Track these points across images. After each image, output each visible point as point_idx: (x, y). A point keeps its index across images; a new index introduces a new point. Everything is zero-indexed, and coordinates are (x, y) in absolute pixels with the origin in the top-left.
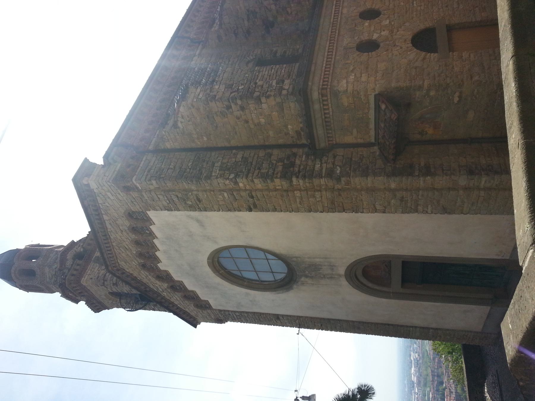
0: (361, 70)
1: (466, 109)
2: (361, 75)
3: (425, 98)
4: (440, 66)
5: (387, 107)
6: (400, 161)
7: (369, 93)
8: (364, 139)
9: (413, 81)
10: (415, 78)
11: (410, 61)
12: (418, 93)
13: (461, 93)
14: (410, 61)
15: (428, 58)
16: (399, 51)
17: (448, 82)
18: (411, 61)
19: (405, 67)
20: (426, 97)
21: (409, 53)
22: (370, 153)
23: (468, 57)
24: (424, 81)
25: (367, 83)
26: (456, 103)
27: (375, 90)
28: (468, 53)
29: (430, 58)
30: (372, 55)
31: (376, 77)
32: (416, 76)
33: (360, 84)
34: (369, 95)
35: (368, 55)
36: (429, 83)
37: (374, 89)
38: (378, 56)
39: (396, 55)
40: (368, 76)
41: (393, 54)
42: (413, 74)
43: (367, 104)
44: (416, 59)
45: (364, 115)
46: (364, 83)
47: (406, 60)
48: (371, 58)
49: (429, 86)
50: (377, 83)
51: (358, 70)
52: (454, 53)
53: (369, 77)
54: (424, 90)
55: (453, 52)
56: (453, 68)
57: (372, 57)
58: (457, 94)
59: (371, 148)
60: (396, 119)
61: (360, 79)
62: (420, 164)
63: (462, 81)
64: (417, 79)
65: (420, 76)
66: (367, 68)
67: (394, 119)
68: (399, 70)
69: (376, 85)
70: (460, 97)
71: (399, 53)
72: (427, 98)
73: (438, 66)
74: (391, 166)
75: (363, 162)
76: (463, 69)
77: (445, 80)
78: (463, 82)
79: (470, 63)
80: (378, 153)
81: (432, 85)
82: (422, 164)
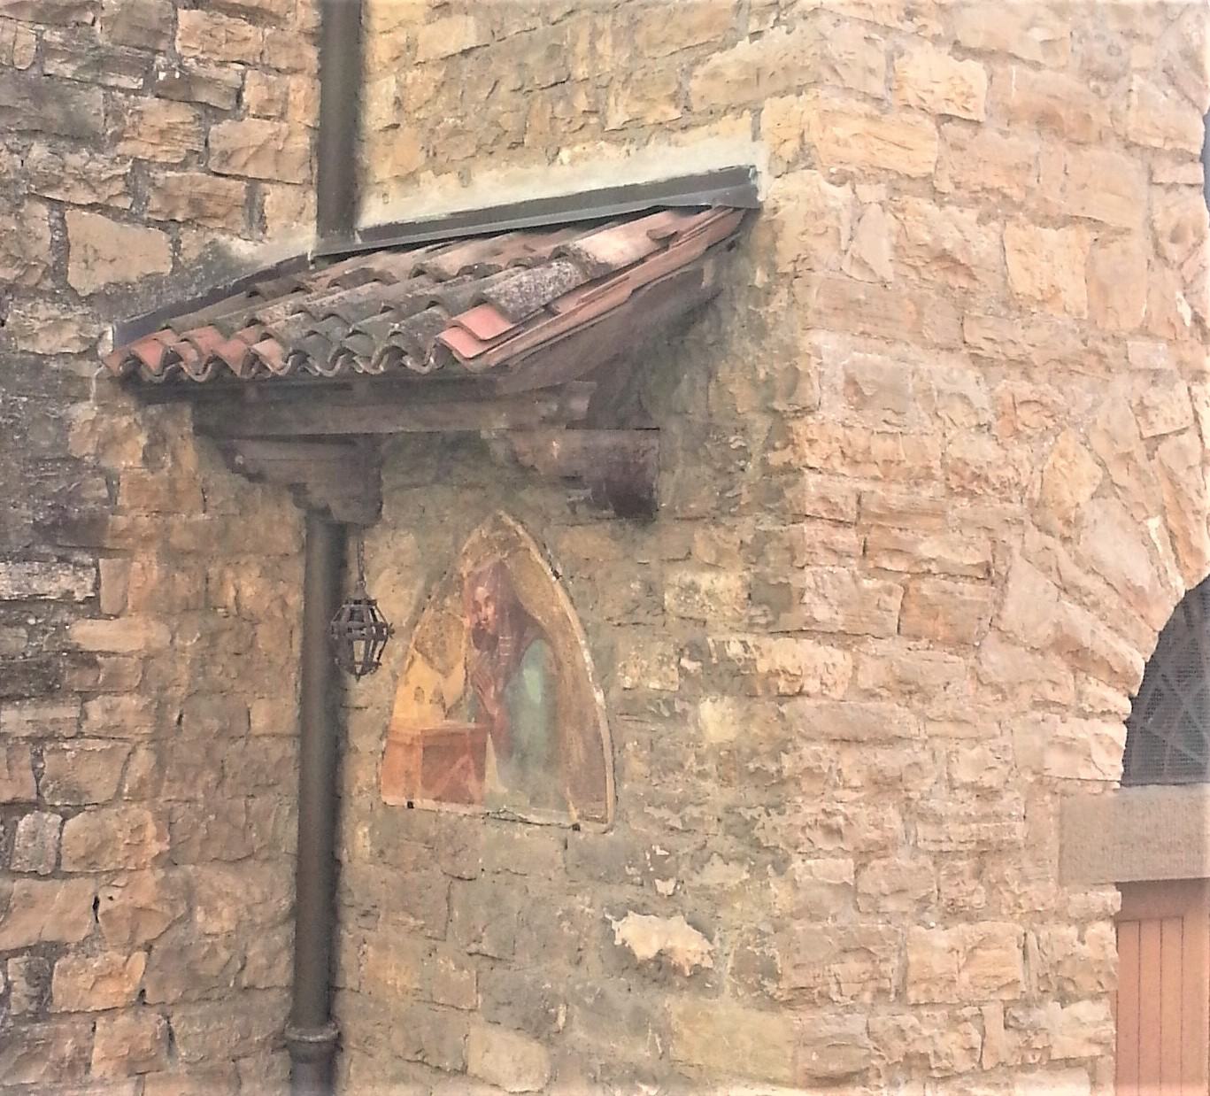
0: (1036, 66)
1: (561, 1020)
2: (976, 54)
3: (681, 653)
4: (986, 794)
5: (601, 275)
6: (143, 440)
7: (773, 109)
8: (396, 126)
9: (848, 539)
10: (885, 564)
11: (1068, 522)
12: (727, 583)
13: (699, 978)
14: (1068, 522)
15: (1080, 694)
16: (1185, 439)
17: (797, 864)
18: (1065, 540)
19: (1009, 473)
20: (692, 658)
21: (1154, 523)
22: (256, 181)
23: (1056, 1055)
24: (845, 638)
25: (879, 100)
26: (611, 934)
27: (791, 166)
28: (1097, 1051)
29: (1087, 717)
30: (1173, 186)
31: (937, 196)
32: (900, 565)
33: (873, 25)
34: (757, 112)
35: (1182, 157)
36: (812, 685)
37: (804, 157)
38: (1156, 245)
39: (1143, 409)
40: (950, 118)
41: (1155, 376)
42: (928, 548)
43: (674, 113)
44: (1087, 582)
45: (582, 103)
46: (878, 61)
47: (1088, 491)
48: (1151, 173)
49: (782, 684)
50: (870, 192)
51: (1038, 34)
52: (1105, 929)
53: (947, 126)
54: (750, 640)
55: (1118, 921)
56: (955, 912)
57: (1151, 183)
58: (687, 946)
59: (312, 197)
60: (445, 351)
61: (936, 39)
62: (92, 608)
63: (802, 997)
64: (870, 576)
65: (895, 603)
66: (1046, 121)
67: (451, 337)
68: (988, 417)
69: (841, 179)
70: (661, 970)
71: (1163, 437)
72: (681, 668)
73: (989, 780)
74: (90, 352)
75: (149, 102)
76: (931, 1004)
77: (833, 832)
78: (789, 1004)
79: (987, 1065)
80: (242, 248)
81: (784, 709)
82: (89, 633)
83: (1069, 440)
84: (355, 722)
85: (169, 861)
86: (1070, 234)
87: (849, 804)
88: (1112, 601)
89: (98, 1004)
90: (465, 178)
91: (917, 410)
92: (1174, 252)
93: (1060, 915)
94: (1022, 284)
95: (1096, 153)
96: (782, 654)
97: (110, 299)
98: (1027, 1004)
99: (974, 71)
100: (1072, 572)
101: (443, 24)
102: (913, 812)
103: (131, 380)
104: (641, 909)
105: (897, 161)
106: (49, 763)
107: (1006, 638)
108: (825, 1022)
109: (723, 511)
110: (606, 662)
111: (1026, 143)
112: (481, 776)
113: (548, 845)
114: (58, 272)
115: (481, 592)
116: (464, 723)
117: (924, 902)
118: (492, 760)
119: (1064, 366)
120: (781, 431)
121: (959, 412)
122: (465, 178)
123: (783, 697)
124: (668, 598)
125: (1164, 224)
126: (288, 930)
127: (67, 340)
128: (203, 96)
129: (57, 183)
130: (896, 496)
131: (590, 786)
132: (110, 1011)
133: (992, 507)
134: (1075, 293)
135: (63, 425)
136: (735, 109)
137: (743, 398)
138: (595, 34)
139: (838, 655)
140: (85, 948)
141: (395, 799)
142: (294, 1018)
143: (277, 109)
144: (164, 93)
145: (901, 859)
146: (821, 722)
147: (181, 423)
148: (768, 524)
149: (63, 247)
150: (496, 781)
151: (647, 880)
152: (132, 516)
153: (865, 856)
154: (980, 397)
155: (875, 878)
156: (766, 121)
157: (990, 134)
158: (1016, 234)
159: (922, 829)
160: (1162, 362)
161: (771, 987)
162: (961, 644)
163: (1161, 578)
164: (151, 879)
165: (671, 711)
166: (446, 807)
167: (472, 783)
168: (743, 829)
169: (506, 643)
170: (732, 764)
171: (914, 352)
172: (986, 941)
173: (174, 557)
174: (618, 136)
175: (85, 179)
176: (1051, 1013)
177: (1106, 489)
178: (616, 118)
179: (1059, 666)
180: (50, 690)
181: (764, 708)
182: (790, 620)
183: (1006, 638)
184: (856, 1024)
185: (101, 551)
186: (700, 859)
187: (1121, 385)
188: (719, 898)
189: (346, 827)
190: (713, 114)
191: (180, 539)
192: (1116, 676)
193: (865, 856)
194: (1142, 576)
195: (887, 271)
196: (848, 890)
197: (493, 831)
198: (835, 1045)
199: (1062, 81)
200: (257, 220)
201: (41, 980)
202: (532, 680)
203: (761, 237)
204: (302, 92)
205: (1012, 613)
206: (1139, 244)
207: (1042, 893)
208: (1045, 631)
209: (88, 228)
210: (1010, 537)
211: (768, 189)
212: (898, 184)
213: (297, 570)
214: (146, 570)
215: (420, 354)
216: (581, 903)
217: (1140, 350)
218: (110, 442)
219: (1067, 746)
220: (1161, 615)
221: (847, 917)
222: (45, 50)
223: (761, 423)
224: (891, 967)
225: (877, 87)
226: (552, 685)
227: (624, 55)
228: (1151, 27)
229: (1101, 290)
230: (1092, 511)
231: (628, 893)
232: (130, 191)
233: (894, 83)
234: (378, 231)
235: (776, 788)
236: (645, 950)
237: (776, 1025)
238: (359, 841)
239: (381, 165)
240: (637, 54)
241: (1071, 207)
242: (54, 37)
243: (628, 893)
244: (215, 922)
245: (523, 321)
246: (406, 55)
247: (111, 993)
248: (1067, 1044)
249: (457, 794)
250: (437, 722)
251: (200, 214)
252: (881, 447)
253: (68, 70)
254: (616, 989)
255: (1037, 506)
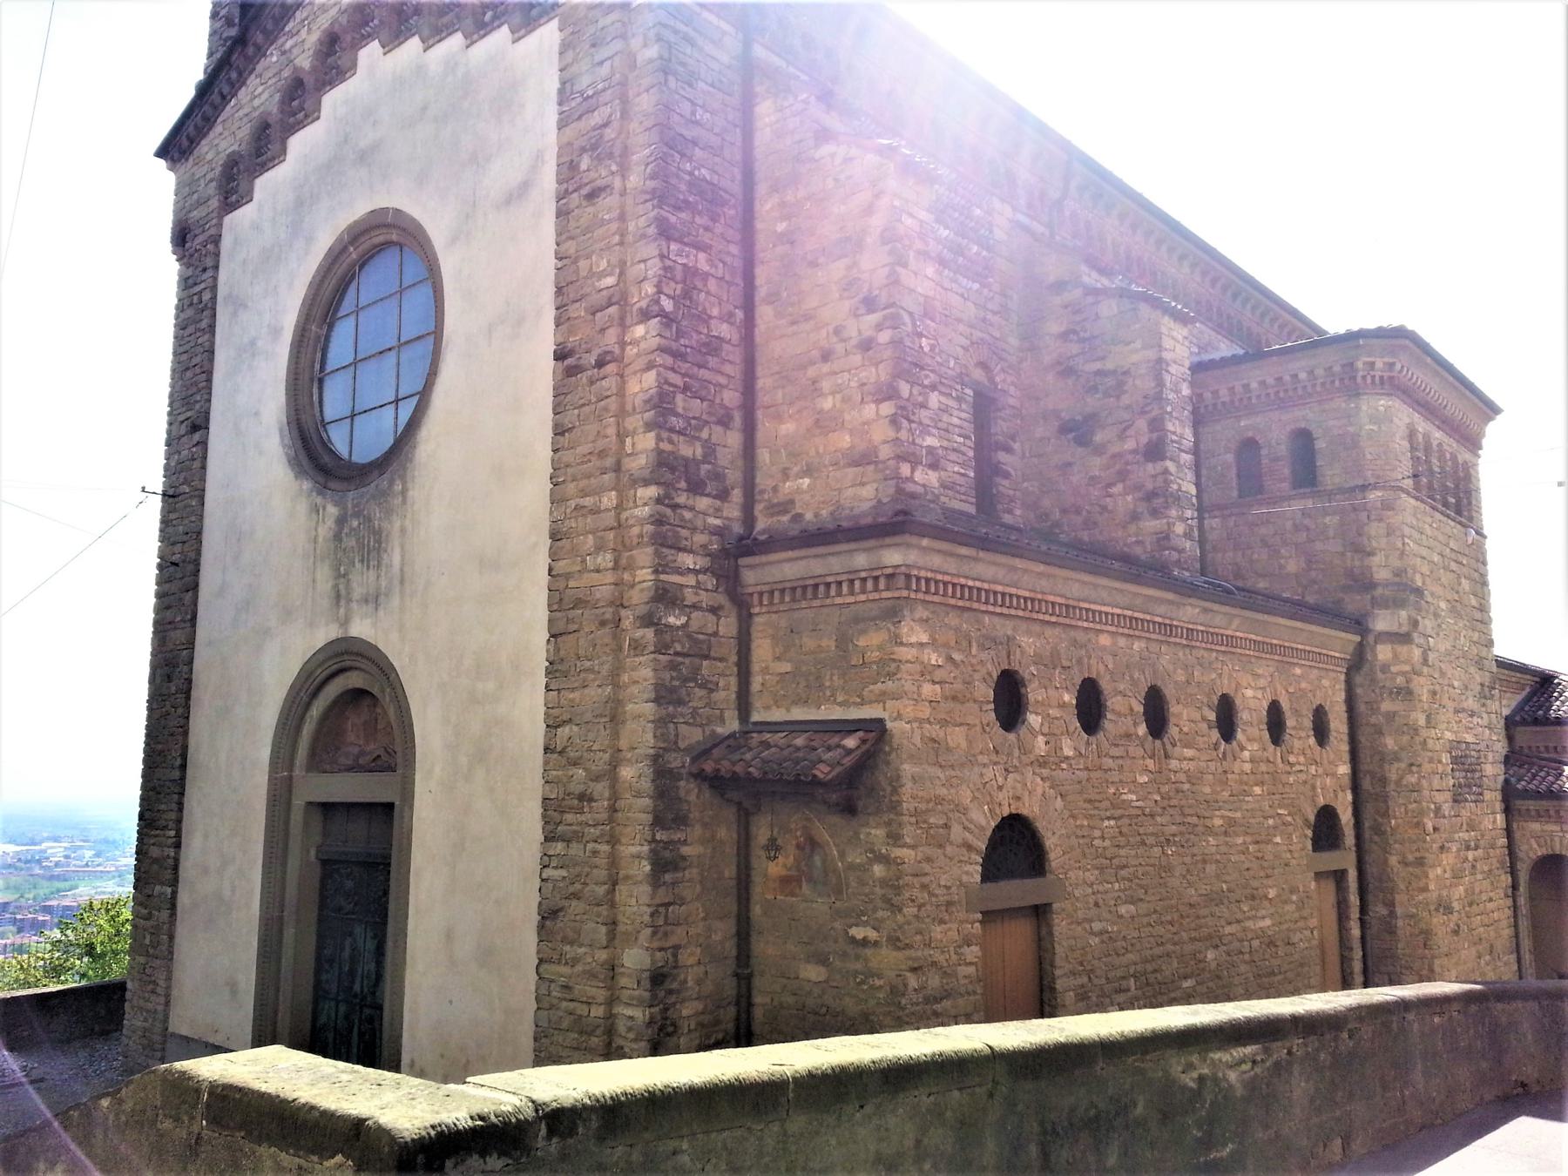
4: (948, 888)
5: (849, 752)
7: (889, 704)
9: (913, 820)
13: (876, 944)
17: (905, 910)
24: (913, 847)
31: (930, 723)
35: (989, 702)
37: (899, 717)
39: (982, 775)
41: (985, 765)
42: (932, 820)
50: (915, 725)
52: (977, 925)
55: (981, 922)
56: (942, 922)
58: (872, 935)
60: (815, 776)
63: (908, 946)
66: (954, 698)
70: (865, 942)
73: (949, 884)
77: (913, 901)
80: (719, 730)
83: (964, 787)
84: (753, 873)
85: (704, 919)
86: (962, 728)
87: (916, 893)
88: (976, 831)
89: (689, 963)
90: (788, 710)
91: (928, 783)
92: (988, 729)
93: (967, 922)
94: (951, 744)
95: (967, 705)
96: (898, 852)
97: (687, 750)
98: (960, 947)
99: (937, 687)
100: (966, 823)
101: (778, 664)
102: (931, 894)
103: (700, 776)
104: (857, 925)
105: (921, 715)
106: (676, 891)
107: (951, 843)
108: (911, 953)
109: (878, 812)
110: (842, 855)
111: (951, 704)
112: (801, 887)
113: (825, 908)
114: (676, 743)
115: (799, 833)
116: (794, 873)
117: (934, 919)
118: (804, 884)
119: (962, 765)
120: (895, 791)
121: (937, 782)
122: (788, 710)
123: (899, 864)
124: (862, 837)
125: (985, 722)
126: (735, 939)
127: (677, 764)
128: (710, 686)
129: (675, 717)
130: (923, 806)
131: (838, 891)
132: (692, 966)
133: (947, 807)
134: (964, 744)
135: (678, 788)
136: (878, 701)
137: (884, 783)
138: (832, 675)
139: (913, 853)
140: (685, 947)
141: (770, 897)
142: (738, 966)
143: (726, 688)
144: (701, 686)
145: (928, 907)
146: (910, 871)
147: (705, 786)
148: (892, 816)
149: (677, 735)
150: (806, 889)
151: (859, 916)
152: (694, 815)
153: (920, 907)
154: (942, 776)
155: (923, 913)
156: (887, 706)
157: (942, 704)
158: (949, 730)
159: (934, 899)
160: (986, 761)
161: (899, 944)
162: (941, 846)
163: (988, 823)
164: (701, 924)
165: (864, 869)
166: (788, 898)
167: (797, 891)
168: (888, 901)
169: (807, 850)
170: (884, 883)
171: (926, 766)
172: (950, 929)
173: (705, 825)
174: (840, 704)
175: (683, 715)
176: (966, 950)
177: (974, 798)
178: (840, 699)
179: (964, 851)
180: (676, 868)
181: (894, 867)
182: (899, 843)
183: (951, 843)
184: (919, 953)
185: (686, 825)
186: (875, 910)
187: (976, 769)
188: (882, 920)
189: (752, 906)
190: (871, 702)
191: (707, 820)
192: (978, 852)
193: (920, 907)
194: (984, 823)
195: (919, 745)
196: (917, 917)
197: (804, 905)
198: (914, 959)
199: (958, 686)
200: (722, 720)
201: (675, 956)
202: (817, 860)
203: (887, 737)
204: (733, 681)
205: (952, 837)
206: (978, 728)
207: (962, 915)
208: (960, 841)
209: (683, 729)
210: (951, 815)
211: (889, 725)
212: (921, 721)
213: (735, 826)
214: (697, 831)
215: (806, 776)
216: (837, 925)
217: (980, 758)
218: (688, 792)
219: (967, 873)
220: (989, 833)
221: (916, 924)
222: (672, 678)
223: (889, 789)
224: (927, 938)
225: (915, 697)
226: (824, 861)
227: (841, 681)
228: (978, 668)
229: (970, 742)
230: (971, 806)
231: (852, 921)
232: (693, 717)
233: (919, 695)
234: (756, 724)
235: (898, 890)
236: (859, 937)
237: (900, 955)
238: (757, 910)
239: (757, 703)
240: (845, 682)
241: (962, 721)
242: (674, 674)
243: (852, 921)
244: (717, 937)
245: (832, 766)
246: (765, 671)
247: (691, 961)
248: (970, 958)
249: (793, 895)
250: (784, 872)
251: (709, 721)
252: (920, 794)
253: (677, 683)
254: (849, 949)
255: (957, 805)
